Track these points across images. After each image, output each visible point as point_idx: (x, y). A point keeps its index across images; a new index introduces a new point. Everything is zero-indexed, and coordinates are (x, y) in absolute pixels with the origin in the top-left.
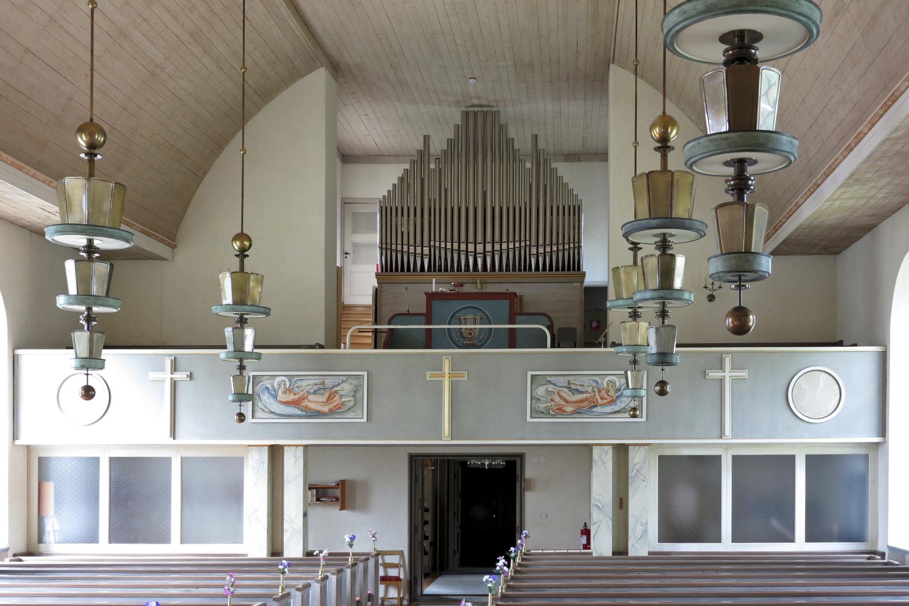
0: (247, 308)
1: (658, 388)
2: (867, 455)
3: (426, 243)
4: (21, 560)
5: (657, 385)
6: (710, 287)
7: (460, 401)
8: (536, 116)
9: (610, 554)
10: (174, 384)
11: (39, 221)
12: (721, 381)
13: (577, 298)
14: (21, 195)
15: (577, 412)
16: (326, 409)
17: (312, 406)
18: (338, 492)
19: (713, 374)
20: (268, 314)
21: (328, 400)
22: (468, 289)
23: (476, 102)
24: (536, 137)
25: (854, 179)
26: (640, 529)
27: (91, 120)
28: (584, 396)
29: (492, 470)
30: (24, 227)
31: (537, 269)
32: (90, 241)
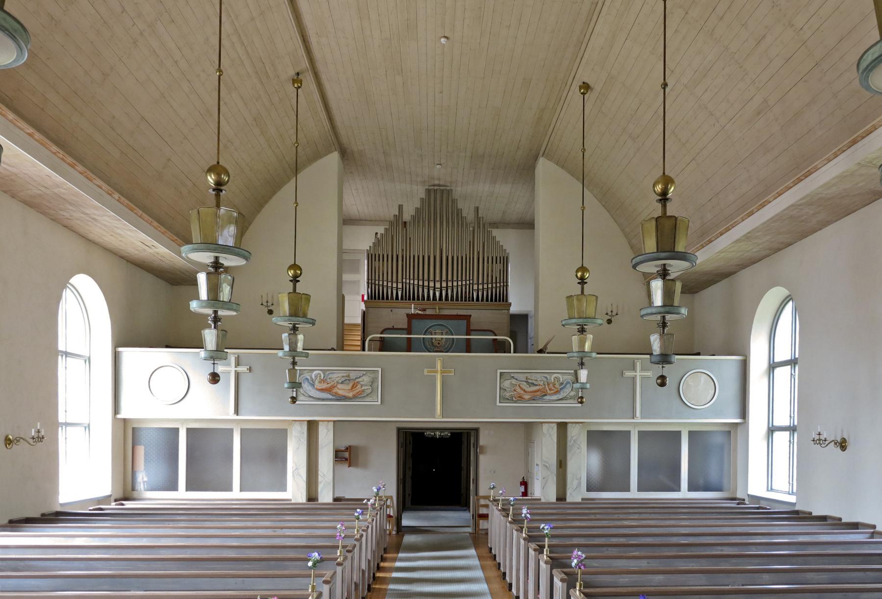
0: (301, 319)
1: (659, 381)
2: (729, 432)
3: (400, 280)
4: (123, 505)
5: (658, 378)
6: (610, 314)
7: (435, 391)
8: (481, 194)
9: (554, 500)
10: (237, 375)
11: (136, 252)
12: (634, 379)
13: (506, 320)
14: (130, 230)
15: (533, 399)
16: (350, 395)
17: (340, 392)
18: (347, 455)
19: (628, 374)
20: (313, 324)
21: (352, 388)
22: (428, 312)
23: (436, 182)
24: (477, 209)
25: (747, 237)
26: (575, 482)
27: (218, 163)
28: (537, 388)
29: (442, 439)
30: (122, 257)
31: (478, 300)
32: (217, 258)
